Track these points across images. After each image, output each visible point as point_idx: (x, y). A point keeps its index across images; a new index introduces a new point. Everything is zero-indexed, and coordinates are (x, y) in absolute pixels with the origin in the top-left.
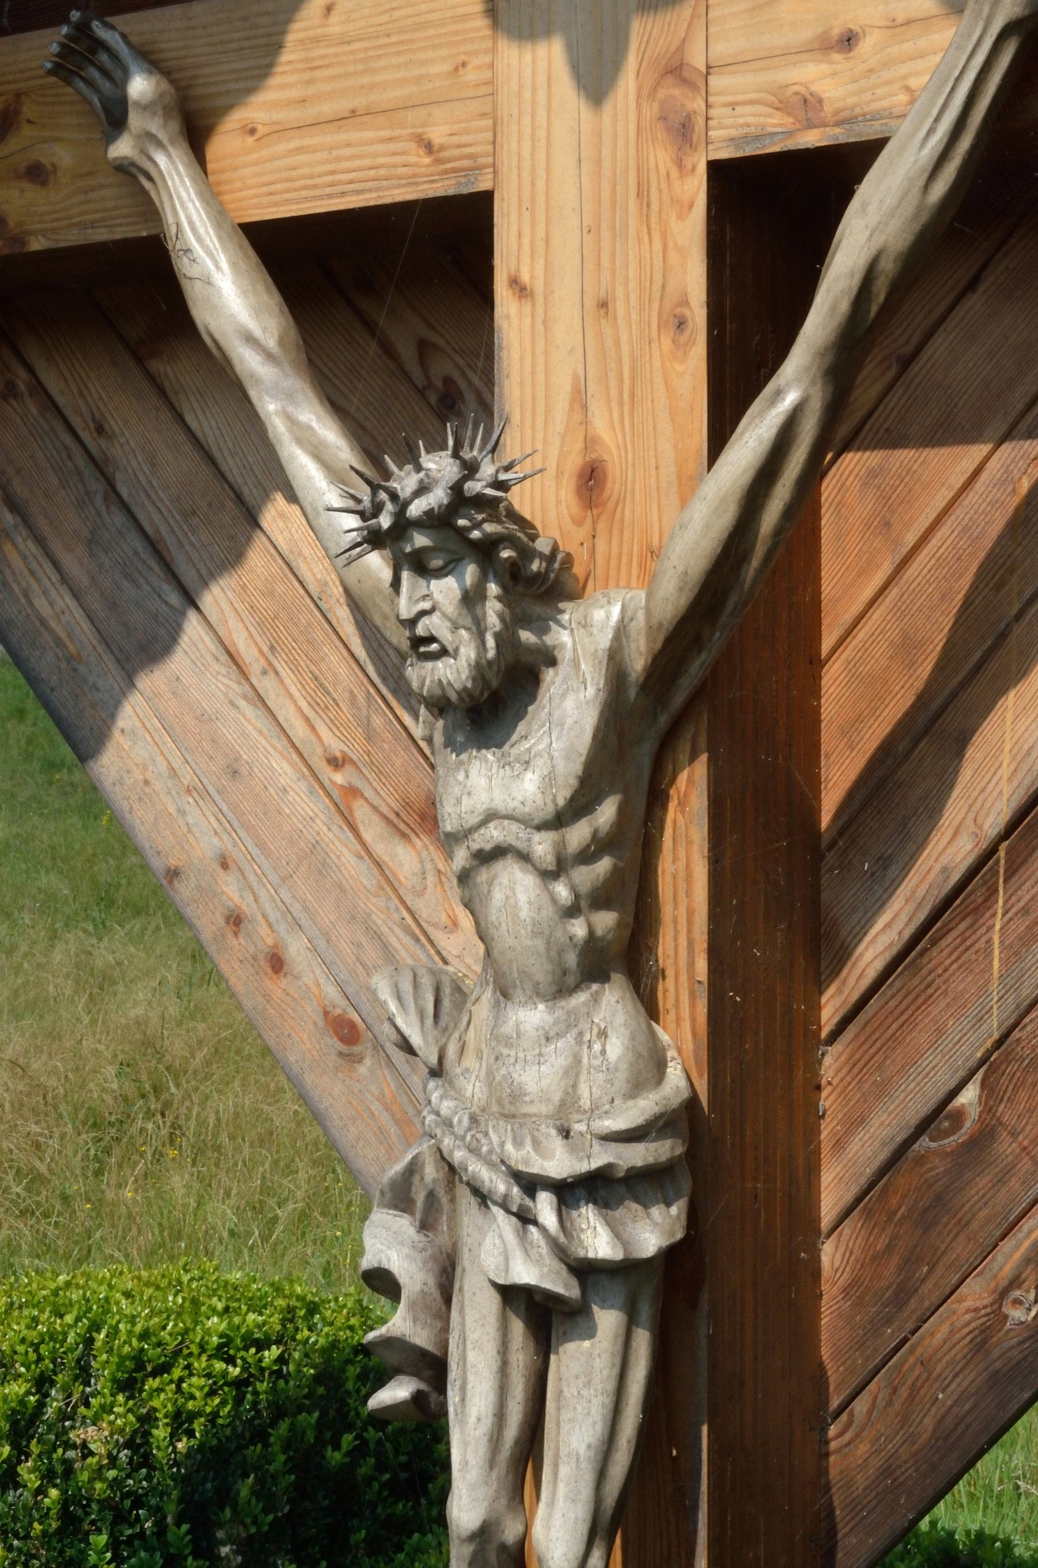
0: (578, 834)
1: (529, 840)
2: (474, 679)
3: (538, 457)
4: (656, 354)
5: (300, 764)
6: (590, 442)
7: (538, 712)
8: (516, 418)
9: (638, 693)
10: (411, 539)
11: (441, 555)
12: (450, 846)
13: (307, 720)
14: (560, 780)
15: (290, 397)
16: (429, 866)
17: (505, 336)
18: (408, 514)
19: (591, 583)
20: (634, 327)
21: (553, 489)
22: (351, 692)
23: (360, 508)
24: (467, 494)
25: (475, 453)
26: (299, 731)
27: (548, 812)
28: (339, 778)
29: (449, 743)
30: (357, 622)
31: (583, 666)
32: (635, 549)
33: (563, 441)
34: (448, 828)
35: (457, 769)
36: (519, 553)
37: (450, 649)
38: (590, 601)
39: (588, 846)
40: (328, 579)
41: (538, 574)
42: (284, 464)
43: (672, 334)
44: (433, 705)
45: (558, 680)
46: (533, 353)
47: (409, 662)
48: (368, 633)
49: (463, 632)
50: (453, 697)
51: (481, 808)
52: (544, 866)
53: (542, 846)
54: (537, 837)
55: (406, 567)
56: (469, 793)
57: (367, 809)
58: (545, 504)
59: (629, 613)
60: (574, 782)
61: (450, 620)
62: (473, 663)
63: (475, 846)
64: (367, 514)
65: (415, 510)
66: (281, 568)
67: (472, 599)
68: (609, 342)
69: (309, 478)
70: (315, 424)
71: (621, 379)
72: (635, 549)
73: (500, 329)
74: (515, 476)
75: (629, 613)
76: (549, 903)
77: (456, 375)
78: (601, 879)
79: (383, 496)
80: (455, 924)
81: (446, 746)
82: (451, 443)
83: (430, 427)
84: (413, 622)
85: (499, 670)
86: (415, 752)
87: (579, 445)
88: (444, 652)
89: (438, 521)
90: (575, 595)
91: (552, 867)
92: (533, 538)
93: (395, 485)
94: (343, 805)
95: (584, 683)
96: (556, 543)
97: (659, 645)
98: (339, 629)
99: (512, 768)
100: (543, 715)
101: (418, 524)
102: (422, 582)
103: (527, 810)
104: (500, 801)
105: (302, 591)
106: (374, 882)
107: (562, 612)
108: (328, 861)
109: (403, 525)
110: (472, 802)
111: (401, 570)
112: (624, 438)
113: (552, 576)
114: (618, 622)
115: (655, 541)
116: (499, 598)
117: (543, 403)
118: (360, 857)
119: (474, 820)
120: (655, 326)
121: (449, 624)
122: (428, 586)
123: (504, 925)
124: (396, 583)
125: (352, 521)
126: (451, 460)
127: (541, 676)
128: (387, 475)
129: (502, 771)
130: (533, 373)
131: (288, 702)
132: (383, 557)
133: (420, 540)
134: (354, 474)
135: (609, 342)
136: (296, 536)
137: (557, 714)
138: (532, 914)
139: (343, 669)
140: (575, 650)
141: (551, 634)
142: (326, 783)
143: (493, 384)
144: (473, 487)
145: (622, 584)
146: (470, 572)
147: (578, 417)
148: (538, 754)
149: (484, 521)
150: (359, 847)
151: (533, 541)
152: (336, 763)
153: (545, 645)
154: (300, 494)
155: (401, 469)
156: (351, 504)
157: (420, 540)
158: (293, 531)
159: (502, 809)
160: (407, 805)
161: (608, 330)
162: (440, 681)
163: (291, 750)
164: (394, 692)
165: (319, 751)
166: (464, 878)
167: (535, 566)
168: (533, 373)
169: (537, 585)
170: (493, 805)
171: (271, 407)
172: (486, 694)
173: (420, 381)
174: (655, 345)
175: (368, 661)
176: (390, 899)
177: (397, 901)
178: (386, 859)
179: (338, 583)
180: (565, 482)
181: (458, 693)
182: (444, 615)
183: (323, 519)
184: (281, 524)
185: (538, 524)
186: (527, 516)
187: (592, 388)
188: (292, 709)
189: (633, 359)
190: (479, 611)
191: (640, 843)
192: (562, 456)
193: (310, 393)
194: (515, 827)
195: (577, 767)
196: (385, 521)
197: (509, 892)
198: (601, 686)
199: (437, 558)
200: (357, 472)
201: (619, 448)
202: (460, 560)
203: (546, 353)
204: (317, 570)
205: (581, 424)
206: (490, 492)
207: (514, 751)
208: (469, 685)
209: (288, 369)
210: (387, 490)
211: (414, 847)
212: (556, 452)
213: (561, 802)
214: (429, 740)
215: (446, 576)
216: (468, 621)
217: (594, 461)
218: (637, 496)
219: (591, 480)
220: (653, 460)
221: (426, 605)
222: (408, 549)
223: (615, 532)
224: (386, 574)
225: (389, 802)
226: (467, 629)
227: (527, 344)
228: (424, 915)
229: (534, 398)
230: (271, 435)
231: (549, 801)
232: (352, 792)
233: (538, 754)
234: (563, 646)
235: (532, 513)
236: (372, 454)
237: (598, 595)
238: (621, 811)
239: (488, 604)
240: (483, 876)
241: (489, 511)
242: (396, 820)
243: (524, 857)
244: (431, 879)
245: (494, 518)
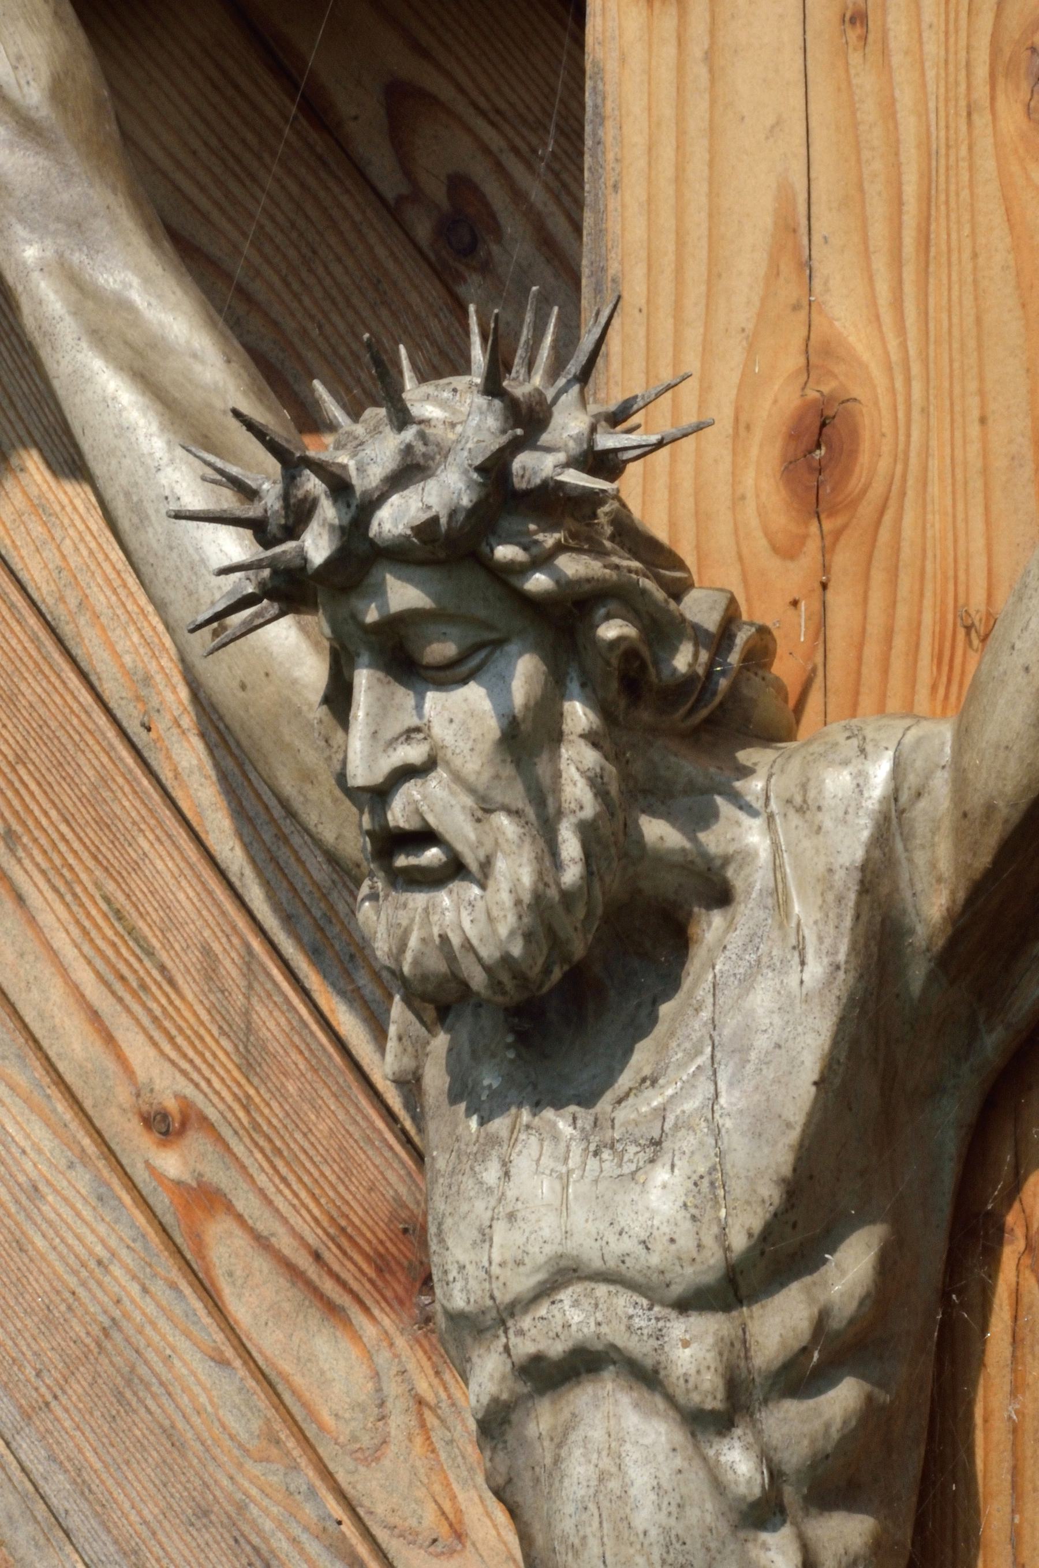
0: (780, 1322)
1: (659, 1334)
2: (528, 937)
3: (689, 391)
4: (985, 143)
5: (74, 1126)
6: (818, 354)
7: (684, 1019)
8: (635, 292)
9: (931, 978)
10: (379, 591)
11: (454, 631)
12: (461, 1345)
13: (94, 1016)
14: (738, 1188)
15: (76, 226)
16: (393, 1388)
17: (610, 89)
18: (374, 530)
19: (815, 699)
20: (931, 74)
21: (725, 466)
22: (207, 951)
23: (253, 511)
24: (520, 484)
25: (537, 380)
26: (73, 1044)
27: (707, 1266)
28: (171, 1163)
29: (461, 1090)
30: (223, 777)
31: (797, 908)
32: (928, 618)
33: (751, 349)
34: (459, 1302)
35: (481, 1156)
36: (643, 630)
37: (471, 862)
38: (816, 748)
39: (805, 1351)
40: (153, 667)
41: (690, 679)
42: (61, 393)
43: (1024, 94)
44: (424, 997)
45: (736, 939)
46: (681, 133)
47: (365, 890)
48: (250, 804)
49: (503, 821)
50: (477, 979)
51: (540, 1253)
52: (696, 1398)
53: (691, 1351)
54: (678, 1327)
55: (365, 658)
56: (511, 1217)
57: (241, 1241)
58: (708, 506)
59: (912, 780)
60: (770, 1193)
61: (471, 790)
62: (527, 898)
63: (524, 1348)
64: (273, 528)
65: (394, 518)
66: (34, 639)
67: (525, 741)
68: (869, 111)
69: (124, 430)
70: (137, 297)
71: (898, 201)
72: (928, 618)
73: (600, 71)
74: (634, 439)
75: (912, 780)
76: (705, 1487)
77: (480, 171)
78: (835, 1434)
79: (313, 484)
80: (459, 1535)
81: (454, 1098)
82: (478, 355)
83: (414, 298)
84: (379, 795)
85: (589, 915)
86: (364, 1103)
87: (793, 361)
88: (455, 869)
89: (447, 549)
90: (775, 734)
91: (715, 1403)
92: (677, 591)
93: (343, 458)
94: (180, 1232)
95: (800, 949)
96: (732, 601)
97: (984, 860)
98: (178, 794)
99: (620, 1157)
100: (697, 1025)
101: (399, 555)
102: (405, 697)
103: (655, 1260)
104: (588, 1237)
105: (86, 697)
106: (256, 1425)
107: (746, 772)
108: (142, 1370)
109: (360, 557)
110: (518, 1237)
111: (352, 666)
112: (904, 346)
113: (723, 683)
114: (884, 800)
115: (977, 601)
116: (592, 738)
117: (703, 254)
118: (223, 1362)
119: (522, 1283)
120: (981, 72)
121: (469, 801)
122: (419, 707)
123: (593, 1544)
124: (339, 697)
125: (231, 546)
126: (481, 401)
127: (693, 930)
128: (311, 421)
129: (592, 1163)
130: (679, 179)
131: (46, 971)
132: (303, 629)
133: (403, 594)
134: (235, 424)
135: (869, 111)
136: (74, 561)
137: (730, 1025)
138: (662, 1517)
139: (188, 893)
140: (777, 867)
141: (718, 828)
142: (140, 1175)
143: (579, 204)
144: (535, 466)
145: (894, 704)
146: (524, 673)
147: (789, 291)
148: (684, 1124)
149: (560, 548)
150: (219, 1337)
151: (677, 597)
152: (164, 1125)
153: (704, 855)
154: (98, 468)
155: (355, 415)
156: (228, 501)
157: (403, 594)
158: (67, 546)
159: (592, 1257)
160: (342, 1233)
161: (866, 81)
162: (444, 938)
163: (53, 1092)
164: (315, 954)
165: (123, 1094)
166: (495, 1425)
167: (683, 659)
168: (679, 179)
169: (686, 707)
170: (571, 1247)
171: (31, 253)
172: (557, 974)
173: (391, 185)
174: (982, 120)
175: (249, 872)
176: (296, 1468)
177: (311, 1473)
178: (287, 1366)
179: (177, 679)
180: (754, 452)
181: (487, 969)
182: (457, 778)
183: (154, 535)
184: (37, 530)
185: (686, 553)
186: (661, 533)
187: (825, 221)
188: (57, 993)
189: (928, 154)
190: (542, 769)
191: (932, 1345)
192: (749, 385)
193: (128, 222)
194: (624, 1301)
195: (779, 1157)
196: (317, 546)
197: (606, 1463)
198: (841, 957)
199: (444, 637)
200: (250, 426)
201: (889, 369)
202: (498, 644)
203: (713, 131)
204: (128, 647)
205: (796, 308)
206: (574, 478)
207: (622, 1114)
208: (517, 949)
209: (72, 159)
210: (320, 469)
211: (356, 1337)
212: (735, 378)
213: (739, 1242)
214: (410, 1085)
215: (464, 681)
216: (516, 795)
217: (827, 400)
218: (934, 489)
219: (820, 446)
220: (974, 402)
221: (413, 753)
222: (372, 616)
223: (878, 577)
224: (312, 671)
225: (296, 1226)
226: (510, 812)
227: (667, 111)
228: (380, 1509)
229: (680, 243)
230: (29, 321)
231: (709, 1240)
232: (205, 1198)
233: (684, 1124)
234: (747, 856)
235: (672, 525)
236: (275, 365)
237: (836, 731)
238: (887, 1264)
239: (565, 752)
240: (542, 1420)
241: (570, 523)
242: (312, 1271)
243: (646, 1377)
244: (399, 1422)
245: (584, 542)
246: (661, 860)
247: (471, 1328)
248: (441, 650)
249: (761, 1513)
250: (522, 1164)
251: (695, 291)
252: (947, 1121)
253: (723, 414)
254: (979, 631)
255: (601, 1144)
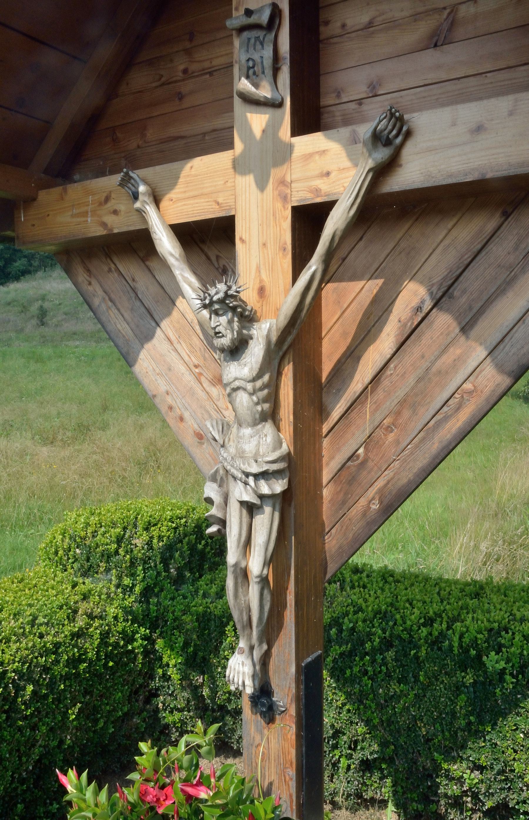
0: (259, 383)
6: (261, 281)
8: (242, 274)
15: (182, 270)
26: (186, 358)
27: (251, 378)
28: (197, 370)
29: (225, 360)
50: (226, 348)
54: (248, 384)
58: (249, 297)
60: (258, 370)
63: (232, 387)
65: (215, 298)
67: (230, 322)
70: (189, 277)
77: (226, 265)
79: (207, 295)
84: (215, 328)
87: (258, 282)
88: (223, 336)
89: (221, 301)
90: (258, 321)
92: (246, 306)
94: (198, 378)
100: (249, 352)
101: (216, 302)
102: (217, 318)
104: (238, 375)
109: (212, 303)
119: (231, 380)
124: (210, 318)
125: (199, 302)
128: (208, 289)
133: (217, 306)
135: (266, 255)
144: (230, 292)
146: (230, 315)
152: (196, 366)
157: (217, 306)
161: (266, 251)
166: (229, 395)
167: (247, 313)
169: (247, 318)
173: (217, 266)
194: (242, 382)
195: (258, 366)
196: (207, 302)
204: (190, 316)
213: (254, 375)
219: (261, 291)
221: (218, 324)
224: (208, 316)
225: (210, 376)
232: (200, 374)
238: (270, 377)
240: (234, 394)
243: (245, 389)
244: (221, 396)
245: (236, 301)
246: (245, 335)
247: (225, 386)
248: (221, 312)
249: (257, 404)
250: (231, 367)
251: (248, 275)
252: (276, 362)
253: (251, 286)
254: (278, 310)
255: (239, 365)
